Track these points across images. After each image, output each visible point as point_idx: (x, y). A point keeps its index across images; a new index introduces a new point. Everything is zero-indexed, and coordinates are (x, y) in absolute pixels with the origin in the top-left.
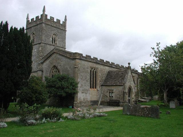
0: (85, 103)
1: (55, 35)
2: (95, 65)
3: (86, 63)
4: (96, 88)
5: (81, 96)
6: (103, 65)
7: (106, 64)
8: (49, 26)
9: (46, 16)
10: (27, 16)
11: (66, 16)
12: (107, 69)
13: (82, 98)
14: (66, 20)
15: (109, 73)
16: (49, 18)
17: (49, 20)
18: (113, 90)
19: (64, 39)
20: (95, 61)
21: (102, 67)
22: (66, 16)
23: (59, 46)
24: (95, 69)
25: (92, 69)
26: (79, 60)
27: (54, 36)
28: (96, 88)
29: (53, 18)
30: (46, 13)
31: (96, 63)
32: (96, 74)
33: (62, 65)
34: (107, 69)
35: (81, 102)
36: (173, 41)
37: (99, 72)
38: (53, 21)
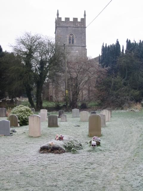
9: (61, 18)
11: (58, 11)
14: (85, 15)
16: (63, 20)
27: (71, 36)
30: (59, 17)
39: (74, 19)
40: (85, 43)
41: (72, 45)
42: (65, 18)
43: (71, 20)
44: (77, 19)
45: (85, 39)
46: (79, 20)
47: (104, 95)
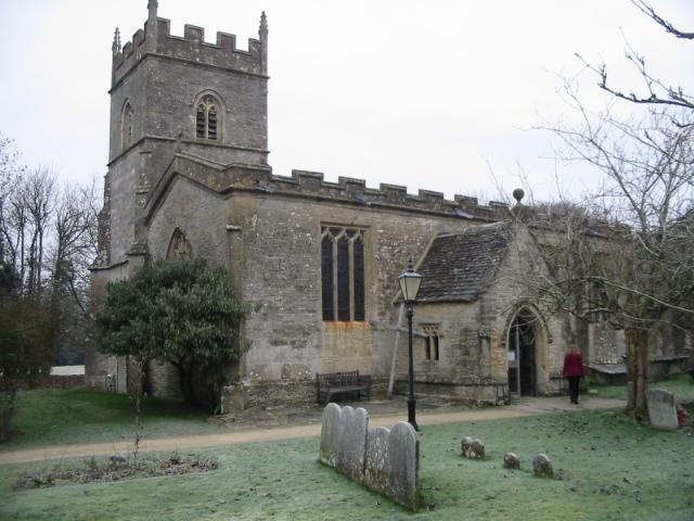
0: (292, 387)
1: (211, 101)
2: (346, 215)
3: (296, 211)
4: (360, 316)
5: (263, 357)
6: (404, 210)
7: (420, 207)
8: (181, 67)
9: (165, 24)
10: (115, 38)
11: (263, 16)
12: (430, 226)
13: (274, 369)
14: (263, 31)
15: (441, 244)
16: (177, 31)
17: (177, 40)
18: (437, 325)
19: (256, 112)
20: (352, 192)
21: (395, 220)
22: (263, 16)
23: (234, 144)
24: (351, 233)
25: (335, 231)
26: (247, 194)
27: (208, 107)
28: (360, 316)
29: (200, 31)
30: (161, 13)
31: (358, 204)
32: (359, 258)
33: (197, 224)
34: (430, 226)
35: (263, 387)
36: (147, 2)
37: (376, 247)
38: (201, 40)
39: (221, 36)
40: (263, 130)
41: (211, 142)
42: (218, 33)
43: (210, 38)
44: (200, 31)
45: (263, 109)
46: (242, 45)
47: (384, 293)
